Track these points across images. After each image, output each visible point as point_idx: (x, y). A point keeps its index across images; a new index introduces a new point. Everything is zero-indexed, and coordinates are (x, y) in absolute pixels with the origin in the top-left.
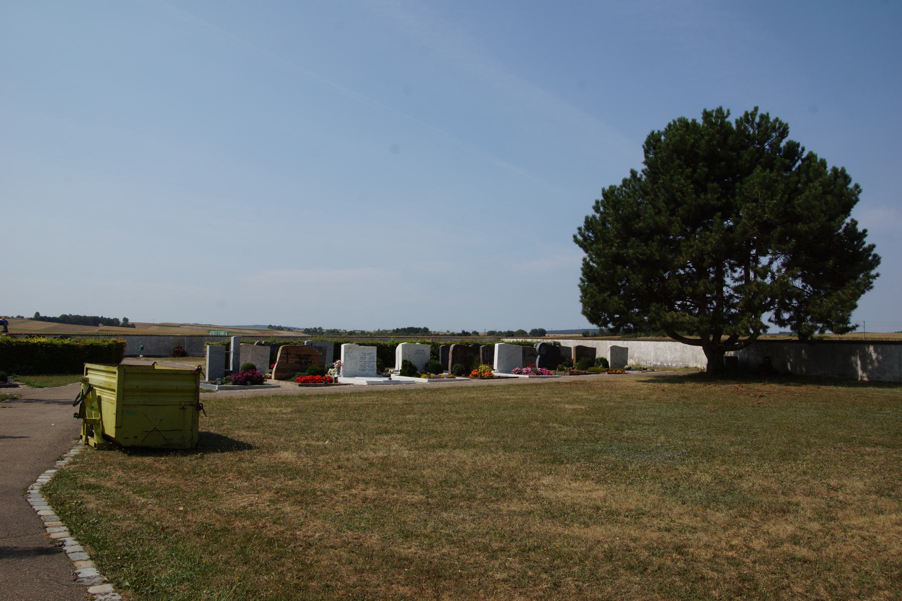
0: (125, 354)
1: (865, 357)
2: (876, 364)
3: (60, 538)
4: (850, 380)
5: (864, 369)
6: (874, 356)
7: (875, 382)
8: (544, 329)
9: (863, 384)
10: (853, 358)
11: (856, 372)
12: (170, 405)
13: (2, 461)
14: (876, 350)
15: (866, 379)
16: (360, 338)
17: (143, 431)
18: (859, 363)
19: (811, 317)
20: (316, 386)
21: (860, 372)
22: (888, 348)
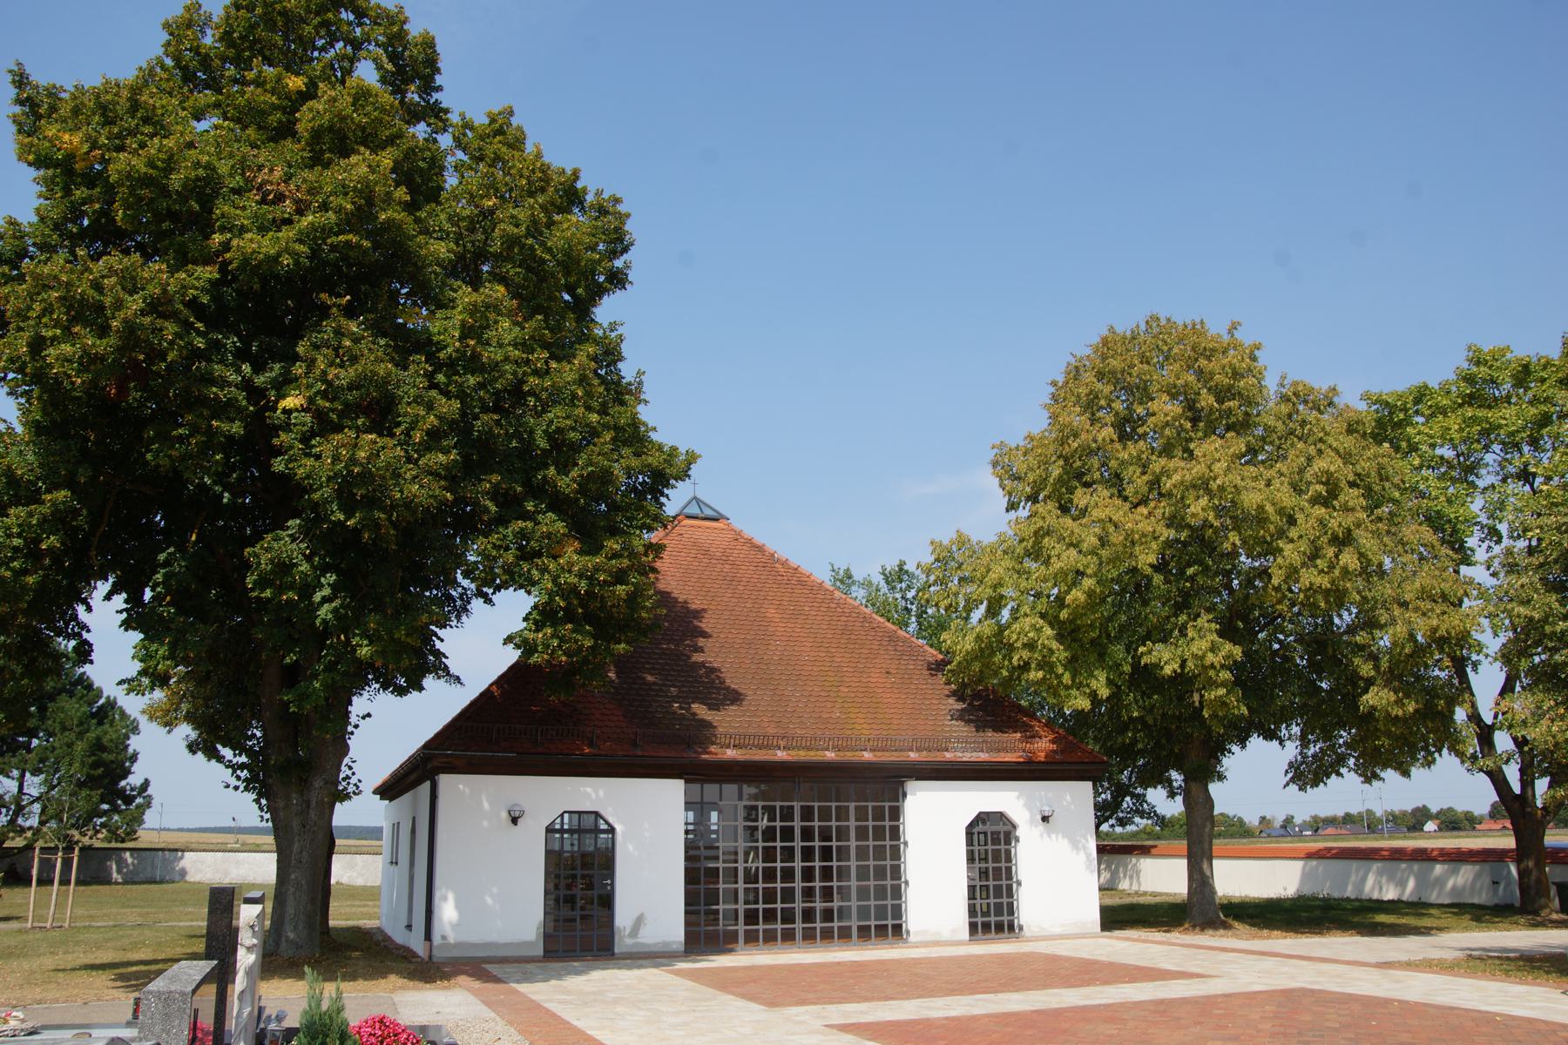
0: (204, 940)
1: (121, 863)
2: (131, 868)
3: (122, 987)
4: (107, 881)
5: (119, 872)
6: (130, 860)
7: (125, 883)
8: (1415, 806)
9: (117, 883)
10: (108, 863)
11: (111, 874)
12: (73, 969)
13: (369, 715)
14: (132, 856)
15: (120, 880)
16: (1095, 797)
17: (353, 774)
18: (114, 867)
19: (117, 783)
20: (947, 1018)
21: (115, 875)
22: (144, 854)
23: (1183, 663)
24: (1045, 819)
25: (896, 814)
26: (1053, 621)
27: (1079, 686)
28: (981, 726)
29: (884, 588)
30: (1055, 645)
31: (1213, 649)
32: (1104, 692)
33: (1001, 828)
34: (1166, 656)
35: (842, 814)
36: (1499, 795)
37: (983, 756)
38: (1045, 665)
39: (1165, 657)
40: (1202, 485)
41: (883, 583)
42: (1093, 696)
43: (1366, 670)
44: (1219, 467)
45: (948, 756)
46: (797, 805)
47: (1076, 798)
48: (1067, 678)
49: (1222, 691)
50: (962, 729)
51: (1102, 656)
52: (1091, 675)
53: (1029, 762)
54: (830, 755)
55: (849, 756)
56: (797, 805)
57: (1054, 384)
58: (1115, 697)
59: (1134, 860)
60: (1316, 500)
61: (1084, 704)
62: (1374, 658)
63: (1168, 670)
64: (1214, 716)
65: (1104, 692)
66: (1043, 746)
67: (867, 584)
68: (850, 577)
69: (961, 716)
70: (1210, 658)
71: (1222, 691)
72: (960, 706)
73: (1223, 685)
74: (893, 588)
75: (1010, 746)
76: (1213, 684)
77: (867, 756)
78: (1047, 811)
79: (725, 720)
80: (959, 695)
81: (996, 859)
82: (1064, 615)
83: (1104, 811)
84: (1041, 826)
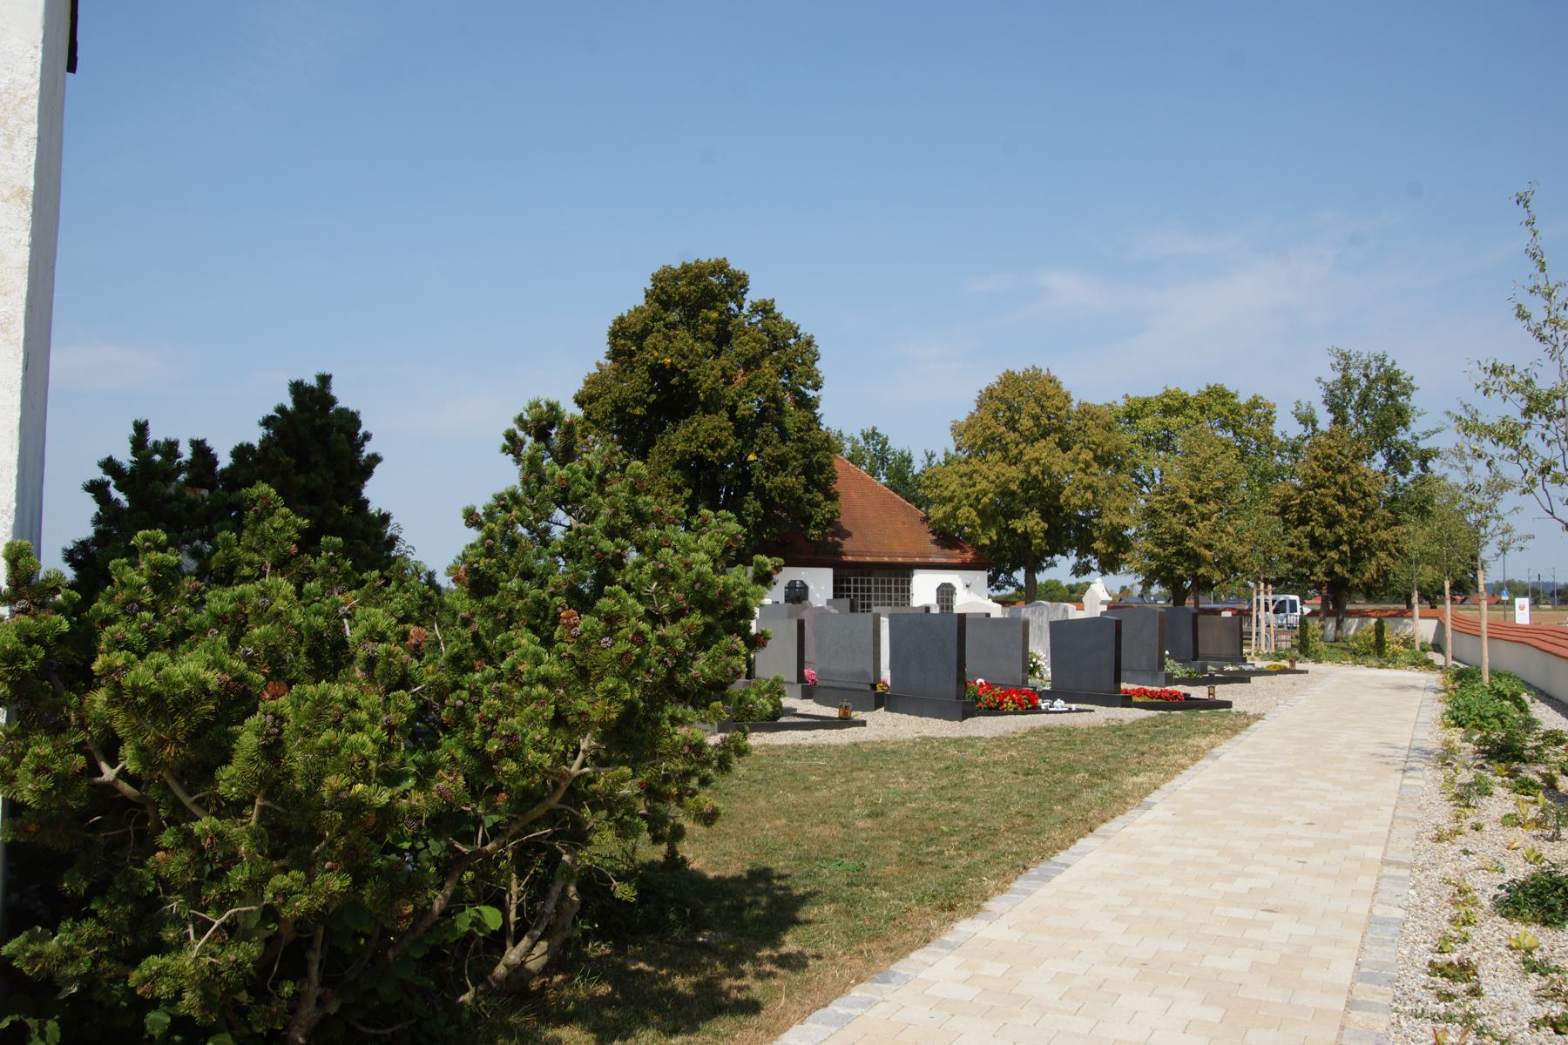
23: (1026, 528)
24: (967, 586)
25: (909, 582)
26: (976, 509)
27: (985, 534)
28: (943, 547)
29: (862, 443)
30: (976, 519)
31: (1038, 524)
32: (995, 538)
33: (950, 589)
34: (1019, 525)
35: (869, 582)
36: (982, 569)
37: (944, 560)
38: (972, 526)
39: (1018, 525)
40: (1037, 461)
41: (861, 439)
42: (991, 538)
43: (1096, 534)
44: (1044, 455)
45: (931, 560)
46: (852, 578)
47: (981, 577)
48: (980, 531)
49: (1039, 541)
50: (934, 548)
51: (995, 522)
52: (990, 530)
53: (963, 563)
54: (886, 559)
55: (893, 560)
56: (852, 578)
57: (980, 391)
58: (1000, 539)
59: (1006, 616)
60: (1081, 469)
61: (987, 542)
62: (1100, 529)
63: (1019, 531)
64: (1036, 549)
65: (995, 538)
66: (969, 556)
67: (851, 439)
68: (841, 435)
69: (935, 542)
70: (1036, 528)
71: (1039, 541)
72: (935, 538)
73: (1040, 538)
74: (868, 443)
75: (956, 556)
76: (1036, 537)
77: (900, 560)
78: (969, 582)
79: (847, 545)
80: (934, 533)
81: (947, 602)
82: (980, 507)
83: (992, 581)
84: (966, 591)
